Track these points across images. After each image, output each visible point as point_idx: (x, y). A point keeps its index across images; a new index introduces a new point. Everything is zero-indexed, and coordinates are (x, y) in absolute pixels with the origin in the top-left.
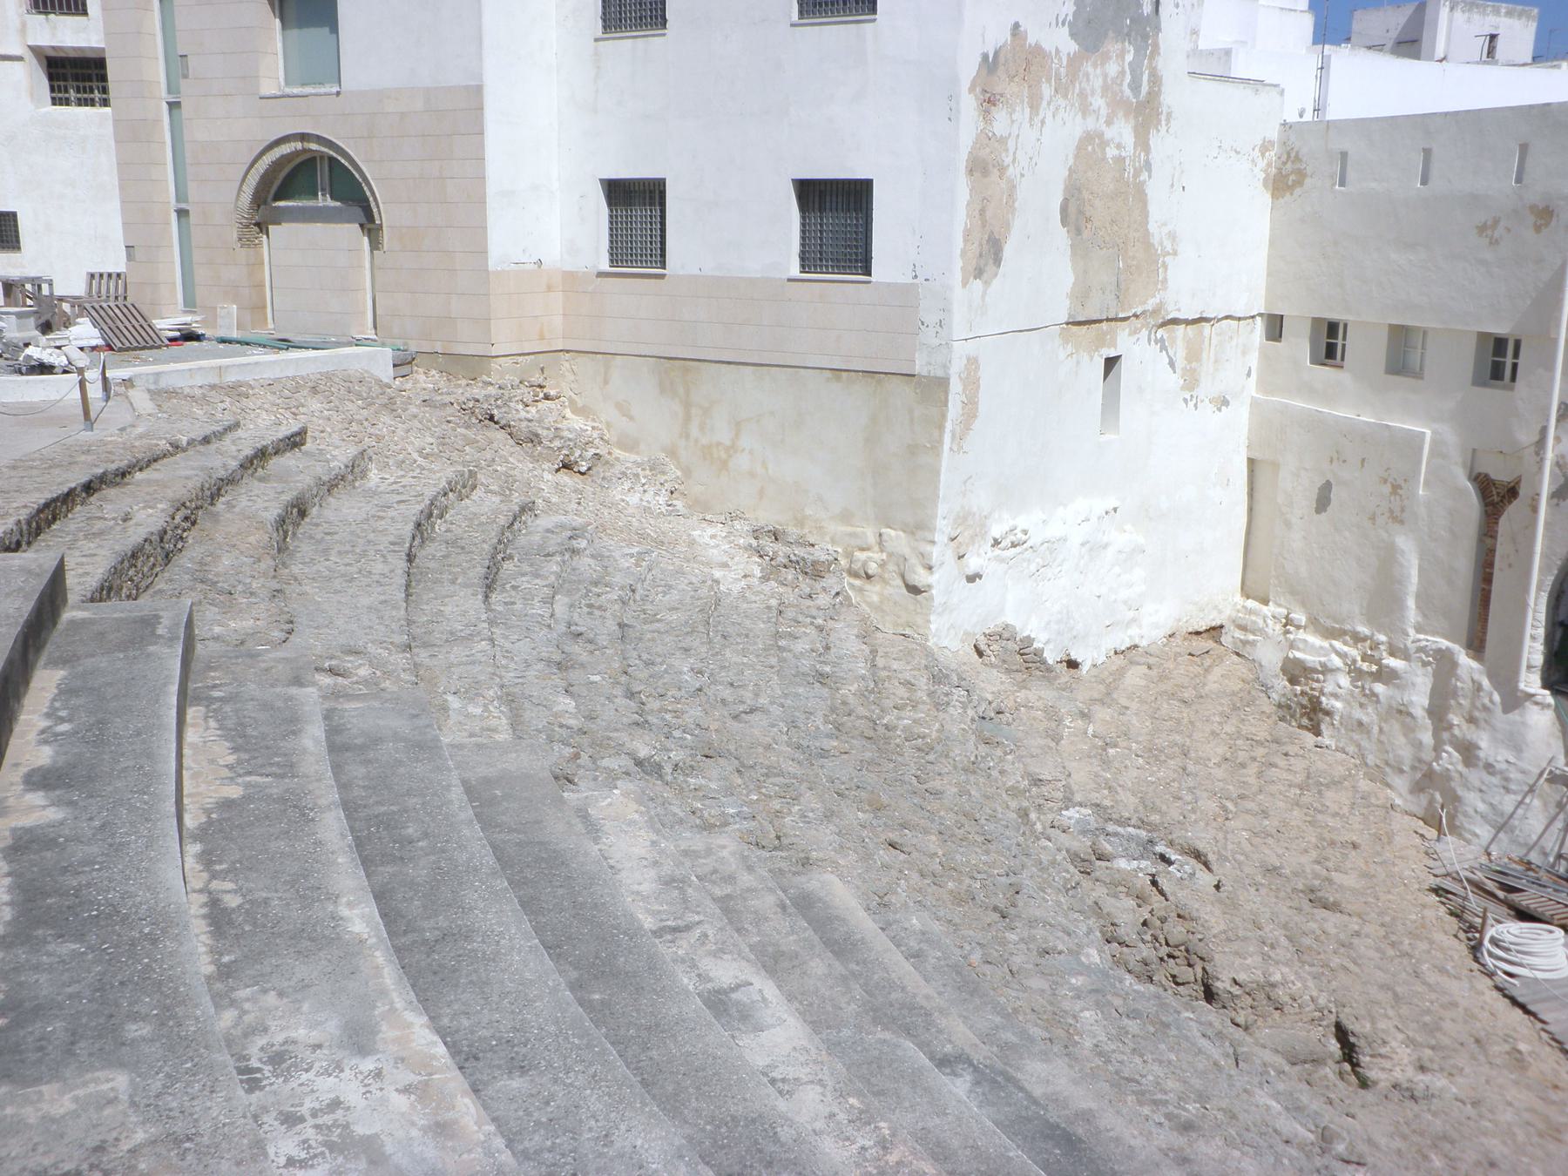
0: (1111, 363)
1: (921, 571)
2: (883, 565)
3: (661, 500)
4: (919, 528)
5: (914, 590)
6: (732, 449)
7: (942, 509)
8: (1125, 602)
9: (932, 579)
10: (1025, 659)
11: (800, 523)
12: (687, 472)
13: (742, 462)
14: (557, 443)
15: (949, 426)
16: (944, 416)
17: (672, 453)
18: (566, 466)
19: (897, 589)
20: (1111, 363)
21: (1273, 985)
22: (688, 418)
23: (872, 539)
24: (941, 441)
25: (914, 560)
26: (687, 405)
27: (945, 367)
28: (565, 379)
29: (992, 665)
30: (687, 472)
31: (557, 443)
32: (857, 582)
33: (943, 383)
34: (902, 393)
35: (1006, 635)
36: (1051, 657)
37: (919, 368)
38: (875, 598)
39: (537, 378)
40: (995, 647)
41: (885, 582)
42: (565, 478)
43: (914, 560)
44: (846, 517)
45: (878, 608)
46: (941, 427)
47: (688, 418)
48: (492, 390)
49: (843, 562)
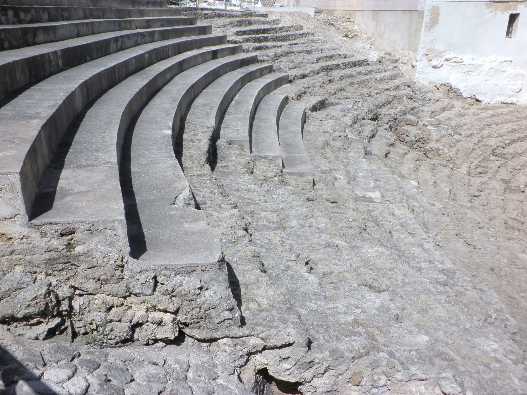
0: (513, 18)
1: (415, 62)
2: (408, 60)
3: (368, 46)
4: (415, 51)
5: (413, 67)
6: (384, 33)
7: (421, 46)
8: (510, 89)
9: (417, 64)
10: (452, 91)
11: (394, 51)
12: (376, 39)
13: (386, 36)
14: (344, 30)
15: (424, 24)
16: (423, 21)
17: (373, 35)
18: (346, 36)
19: (410, 67)
20: (513, 18)
21: (439, 150)
22: (377, 26)
23: (407, 54)
24: (421, 28)
25: (413, 59)
26: (377, 22)
27: (423, 8)
28: (358, 18)
29: (441, 92)
30: (376, 39)
31: (344, 30)
32: (402, 65)
33: (422, 12)
34: (415, 14)
35: (447, 85)
36: (465, 95)
37: (419, 9)
38: (405, 69)
39: (348, 16)
40: (442, 87)
41: (408, 65)
42: (345, 38)
43: (413, 59)
44: (403, 49)
45: (406, 71)
46: (422, 24)
47: (377, 26)
48: (334, 18)
49: (401, 60)
